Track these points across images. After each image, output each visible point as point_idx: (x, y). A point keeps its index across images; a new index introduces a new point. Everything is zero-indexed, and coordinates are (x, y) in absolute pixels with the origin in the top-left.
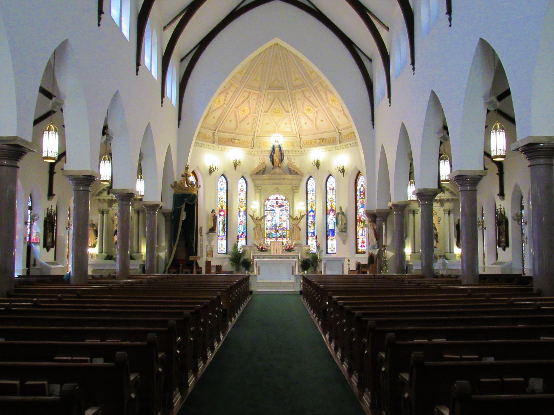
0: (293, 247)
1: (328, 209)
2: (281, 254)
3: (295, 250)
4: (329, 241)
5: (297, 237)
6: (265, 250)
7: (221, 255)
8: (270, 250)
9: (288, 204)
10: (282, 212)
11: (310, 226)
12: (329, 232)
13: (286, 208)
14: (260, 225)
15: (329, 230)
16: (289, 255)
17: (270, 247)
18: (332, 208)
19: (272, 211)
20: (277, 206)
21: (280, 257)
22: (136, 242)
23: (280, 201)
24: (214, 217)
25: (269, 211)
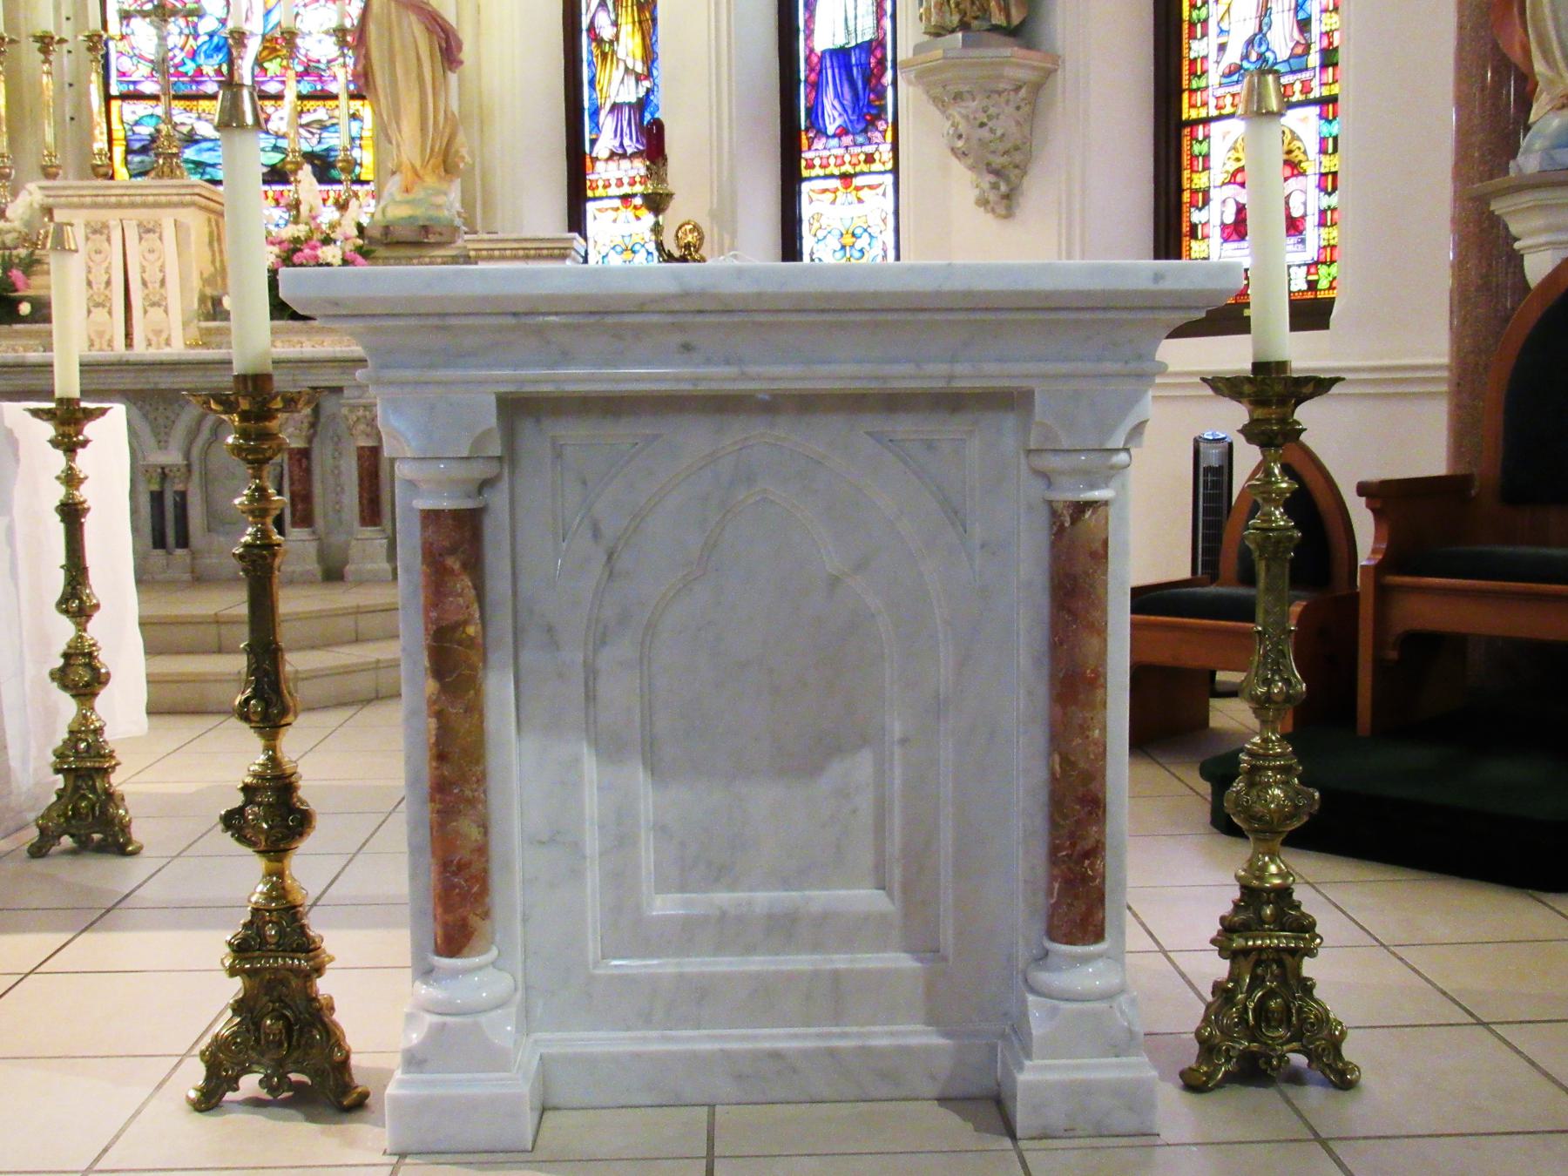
4: (814, 202)
11: (607, 32)
22: (444, 1156)
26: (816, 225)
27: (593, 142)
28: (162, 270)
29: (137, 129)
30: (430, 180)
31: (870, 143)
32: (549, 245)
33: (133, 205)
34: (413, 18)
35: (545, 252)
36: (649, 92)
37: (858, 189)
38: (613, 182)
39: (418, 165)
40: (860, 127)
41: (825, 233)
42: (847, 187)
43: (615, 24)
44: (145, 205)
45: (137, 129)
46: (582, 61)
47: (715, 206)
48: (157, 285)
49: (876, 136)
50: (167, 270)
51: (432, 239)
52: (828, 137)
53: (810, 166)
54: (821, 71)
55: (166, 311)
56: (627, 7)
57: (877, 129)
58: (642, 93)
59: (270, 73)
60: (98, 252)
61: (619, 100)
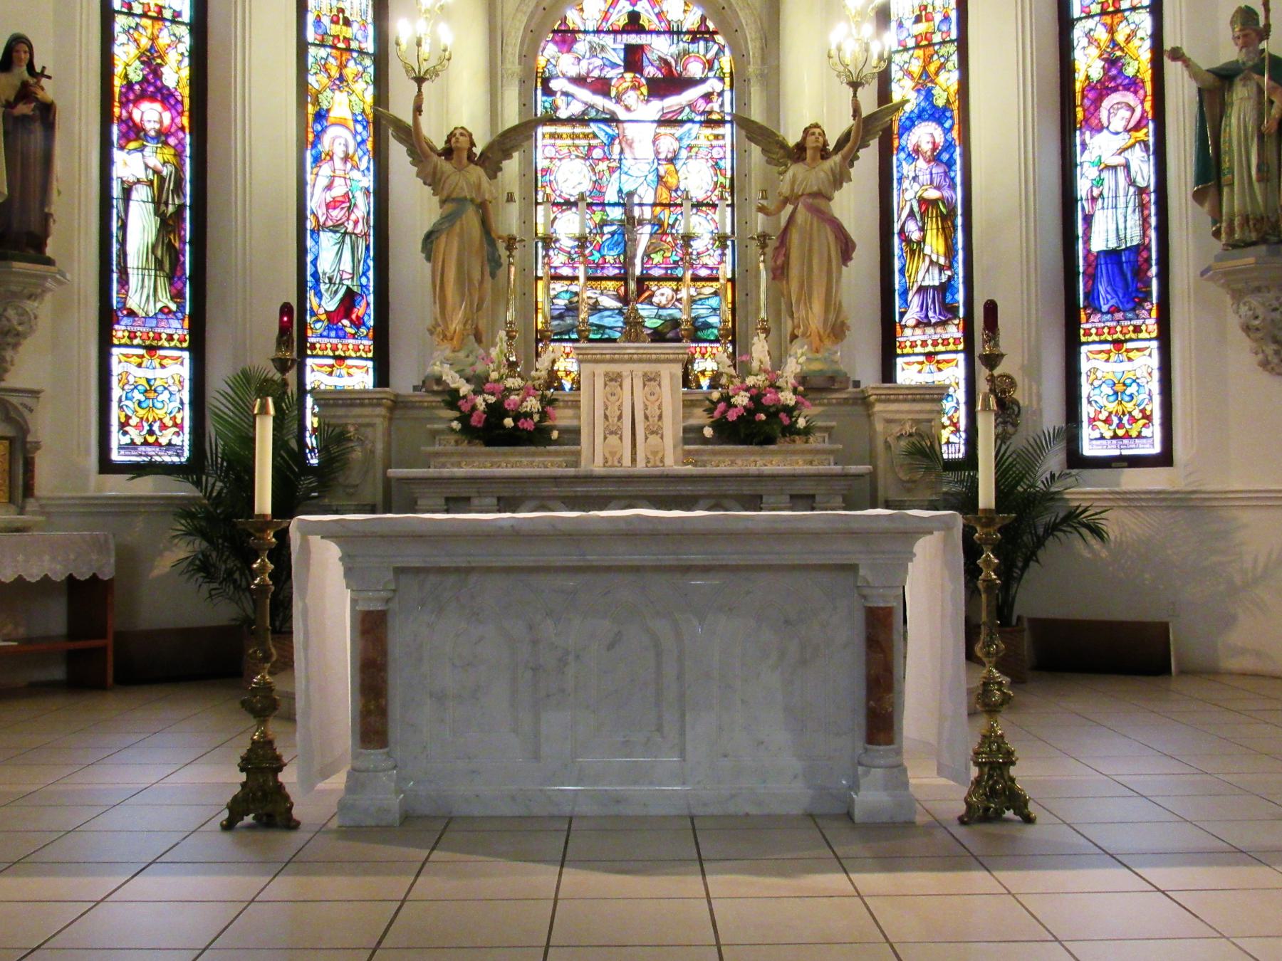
0: (788, 398)
1: (1080, 77)
2: (672, 463)
3: (807, 432)
4: (1091, 361)
5: (815, 316)
6: (528, 425)
7: (145, 486)
8: (572, 435)
9: (726, 62)
10: (678, 131)
11: (916, 236)
12: (1092, 277)
13: (707, 97)
14: (483, 208)
15: (1095, 260)
16: (760, 477)
17: (576, 405)
18: (1112, 63)
19: (593, 127)
20: (635, 87)
21: (673, 489)
23: (661, 47)
24: (24, 109)
25: (571, 121)
26: (1092, 377)
27: (902, 314)
28: (660, 407)
29: (555, 301)
30: (827, 342)
31: (1138, 318)
32: (896, 392)
33: (640, 361)
34: (828, 229)
35: (892, 397)
36: (950, 278)
37: (1128, 351)
38: (919, 343)
39: (822, 331)
40: (1129, 306)
41: (1100, 382)
42: (1119, 350)
43: (922, 229)
44: (650, 361)
45: (555, 301)
46: (191, 182)
47: (1026, 362)
48: (656, 419)
49: (1144, 313)
50: (664, 408)
51: (836, 386)
52: (1103, 313)
53: (1087, 333)
54: (1097, 266)
55: (662, 438)
56: (932, 217)
57: (1144, 308)
58: (944, 279)
59: (655, 262)
60: (613, 394)
61: (924, 284)
